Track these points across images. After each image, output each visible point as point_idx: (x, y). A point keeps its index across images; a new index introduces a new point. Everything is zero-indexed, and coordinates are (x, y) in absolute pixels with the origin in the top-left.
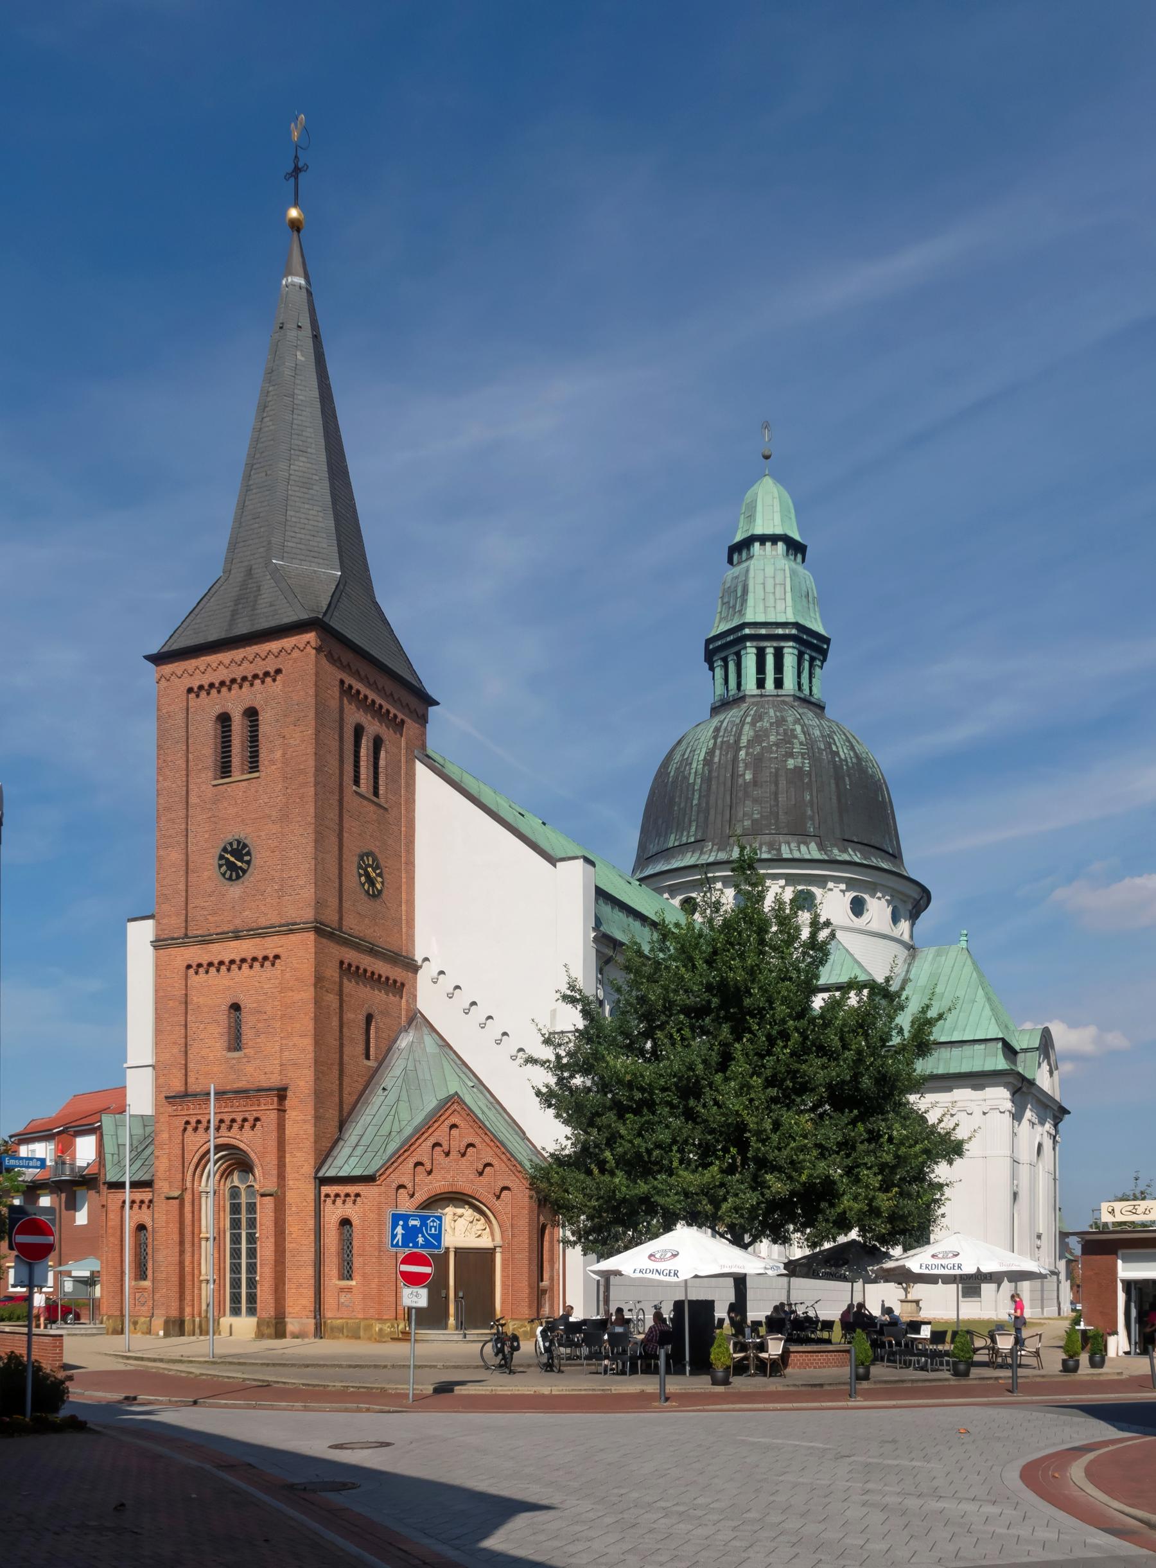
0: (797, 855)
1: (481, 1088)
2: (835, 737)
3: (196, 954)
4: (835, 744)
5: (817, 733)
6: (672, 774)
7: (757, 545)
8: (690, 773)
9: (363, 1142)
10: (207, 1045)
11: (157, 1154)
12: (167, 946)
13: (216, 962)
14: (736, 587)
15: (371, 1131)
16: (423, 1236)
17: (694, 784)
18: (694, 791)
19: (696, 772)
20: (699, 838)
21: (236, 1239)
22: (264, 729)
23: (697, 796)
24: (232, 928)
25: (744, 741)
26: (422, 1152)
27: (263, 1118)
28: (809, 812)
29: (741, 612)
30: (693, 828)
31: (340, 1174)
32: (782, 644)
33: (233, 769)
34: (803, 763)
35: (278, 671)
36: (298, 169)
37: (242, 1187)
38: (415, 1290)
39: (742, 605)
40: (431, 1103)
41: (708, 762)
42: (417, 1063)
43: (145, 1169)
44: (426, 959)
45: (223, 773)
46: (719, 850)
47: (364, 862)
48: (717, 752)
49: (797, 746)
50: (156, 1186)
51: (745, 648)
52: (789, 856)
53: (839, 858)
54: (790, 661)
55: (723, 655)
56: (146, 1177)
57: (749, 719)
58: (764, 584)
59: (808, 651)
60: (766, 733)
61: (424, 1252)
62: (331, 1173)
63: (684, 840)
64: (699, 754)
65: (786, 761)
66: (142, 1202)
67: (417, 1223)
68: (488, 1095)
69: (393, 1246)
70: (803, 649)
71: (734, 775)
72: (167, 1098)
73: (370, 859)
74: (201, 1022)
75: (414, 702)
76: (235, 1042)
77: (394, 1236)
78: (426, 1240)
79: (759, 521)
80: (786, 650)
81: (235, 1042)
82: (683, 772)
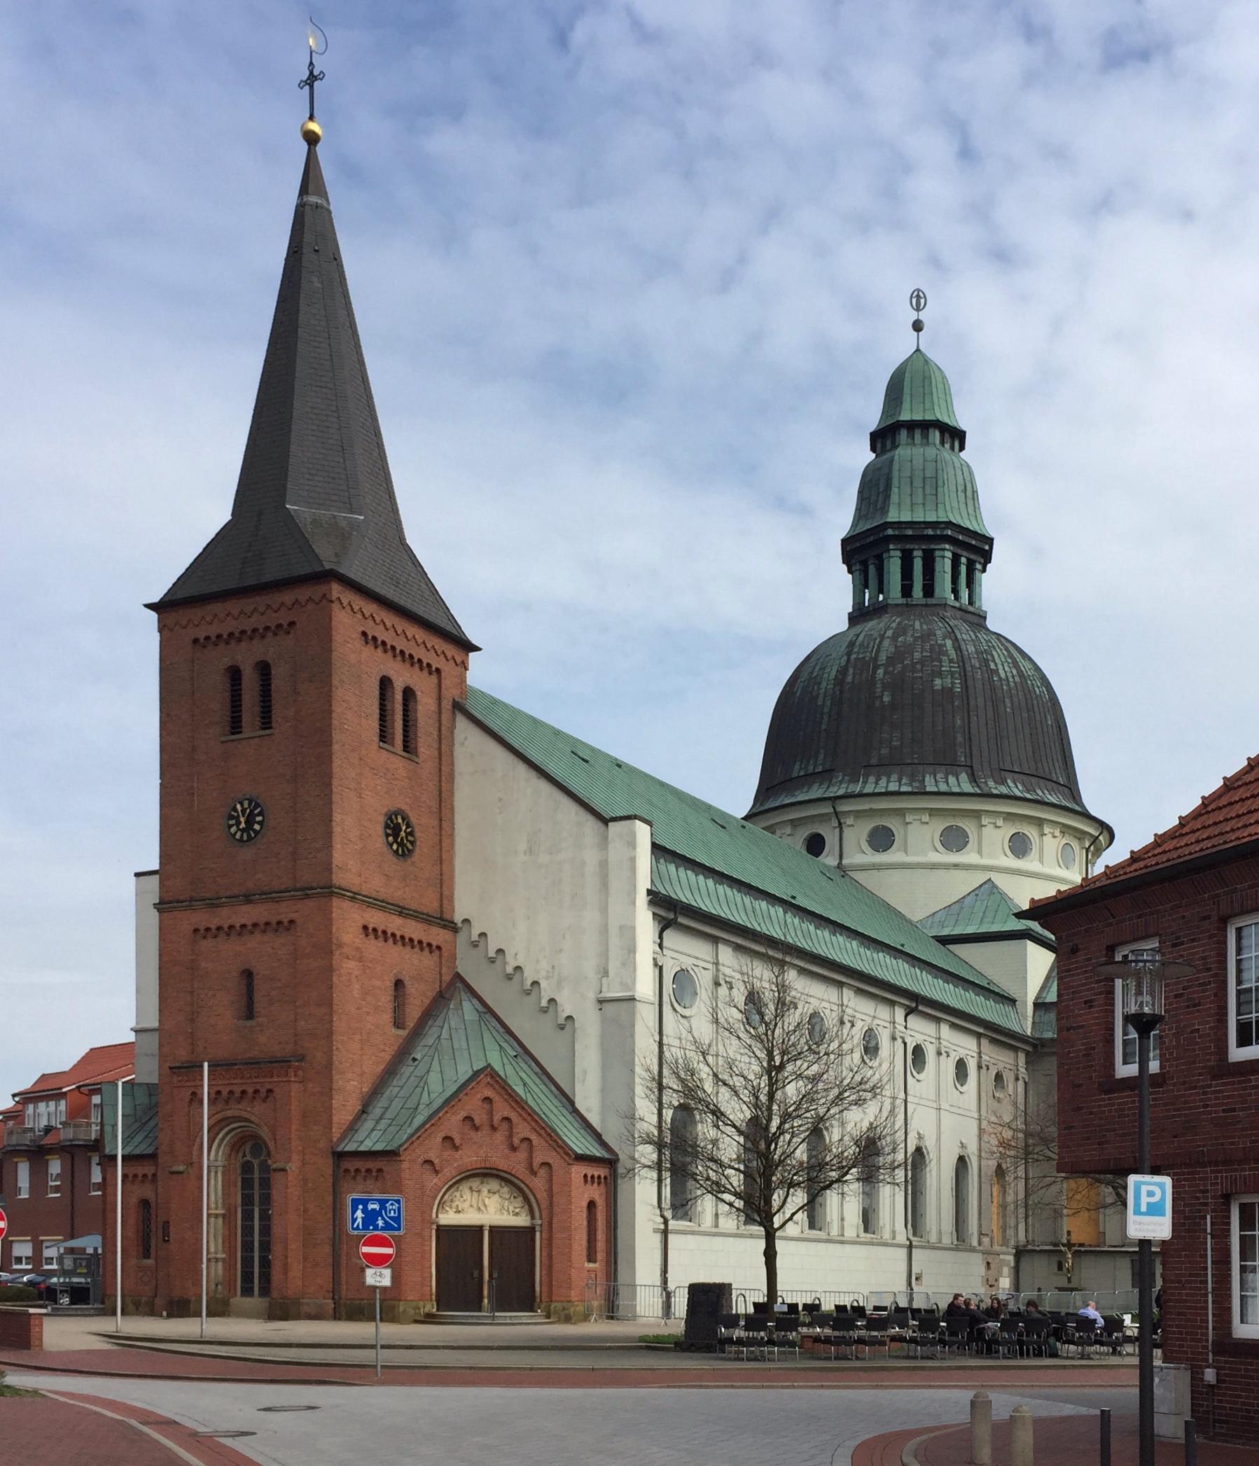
1: (527, 1058)
2: (994, 653)
3: (201, 918)
4: (994, 661)
5: (971, 649)
7: (904, 434)
10: (216, 1013)
11: (160, 1126)
12: (170, 910)
13: (226, 926)
14: (879, 480)
15: (397, 1104)
16: (383, 1219)
18: (822, 714)
20: (827, 767)
21: (247, 1216)
22: (275, 684)
27: (277, 1090)
29: (884, 510)
30: (821, 756)
31: (362, 1148)
32: (933, 546)
33: (244, 725)
34: (953, 683)
35: (292, 624)
36: (314, 76)
38: (379, 1270)
40: (464, 1072)
43: (149, 1141)
45: (233, 728)
46: (850, 781)
47: (392, 822)
48: (851, 671)
50: (160, 1160)
53: (995, 792)
56: (150, 1151)
57: (889, 633)
58: (911, 477)
59: (965, 553)
60: (910, 649)
61: (386, 1234)
62: (351, 1147)
64: (829, 673)
65: (932, 681)
67: (376, 1207)
68: (533, 1064)
69: (353, 1229)
70: (959, 551)
72: (171, 1068)
73: (399, 817)
75: (451, 650)
77: (354, 1220)
78: (386, 1222)
80: (916, 553)
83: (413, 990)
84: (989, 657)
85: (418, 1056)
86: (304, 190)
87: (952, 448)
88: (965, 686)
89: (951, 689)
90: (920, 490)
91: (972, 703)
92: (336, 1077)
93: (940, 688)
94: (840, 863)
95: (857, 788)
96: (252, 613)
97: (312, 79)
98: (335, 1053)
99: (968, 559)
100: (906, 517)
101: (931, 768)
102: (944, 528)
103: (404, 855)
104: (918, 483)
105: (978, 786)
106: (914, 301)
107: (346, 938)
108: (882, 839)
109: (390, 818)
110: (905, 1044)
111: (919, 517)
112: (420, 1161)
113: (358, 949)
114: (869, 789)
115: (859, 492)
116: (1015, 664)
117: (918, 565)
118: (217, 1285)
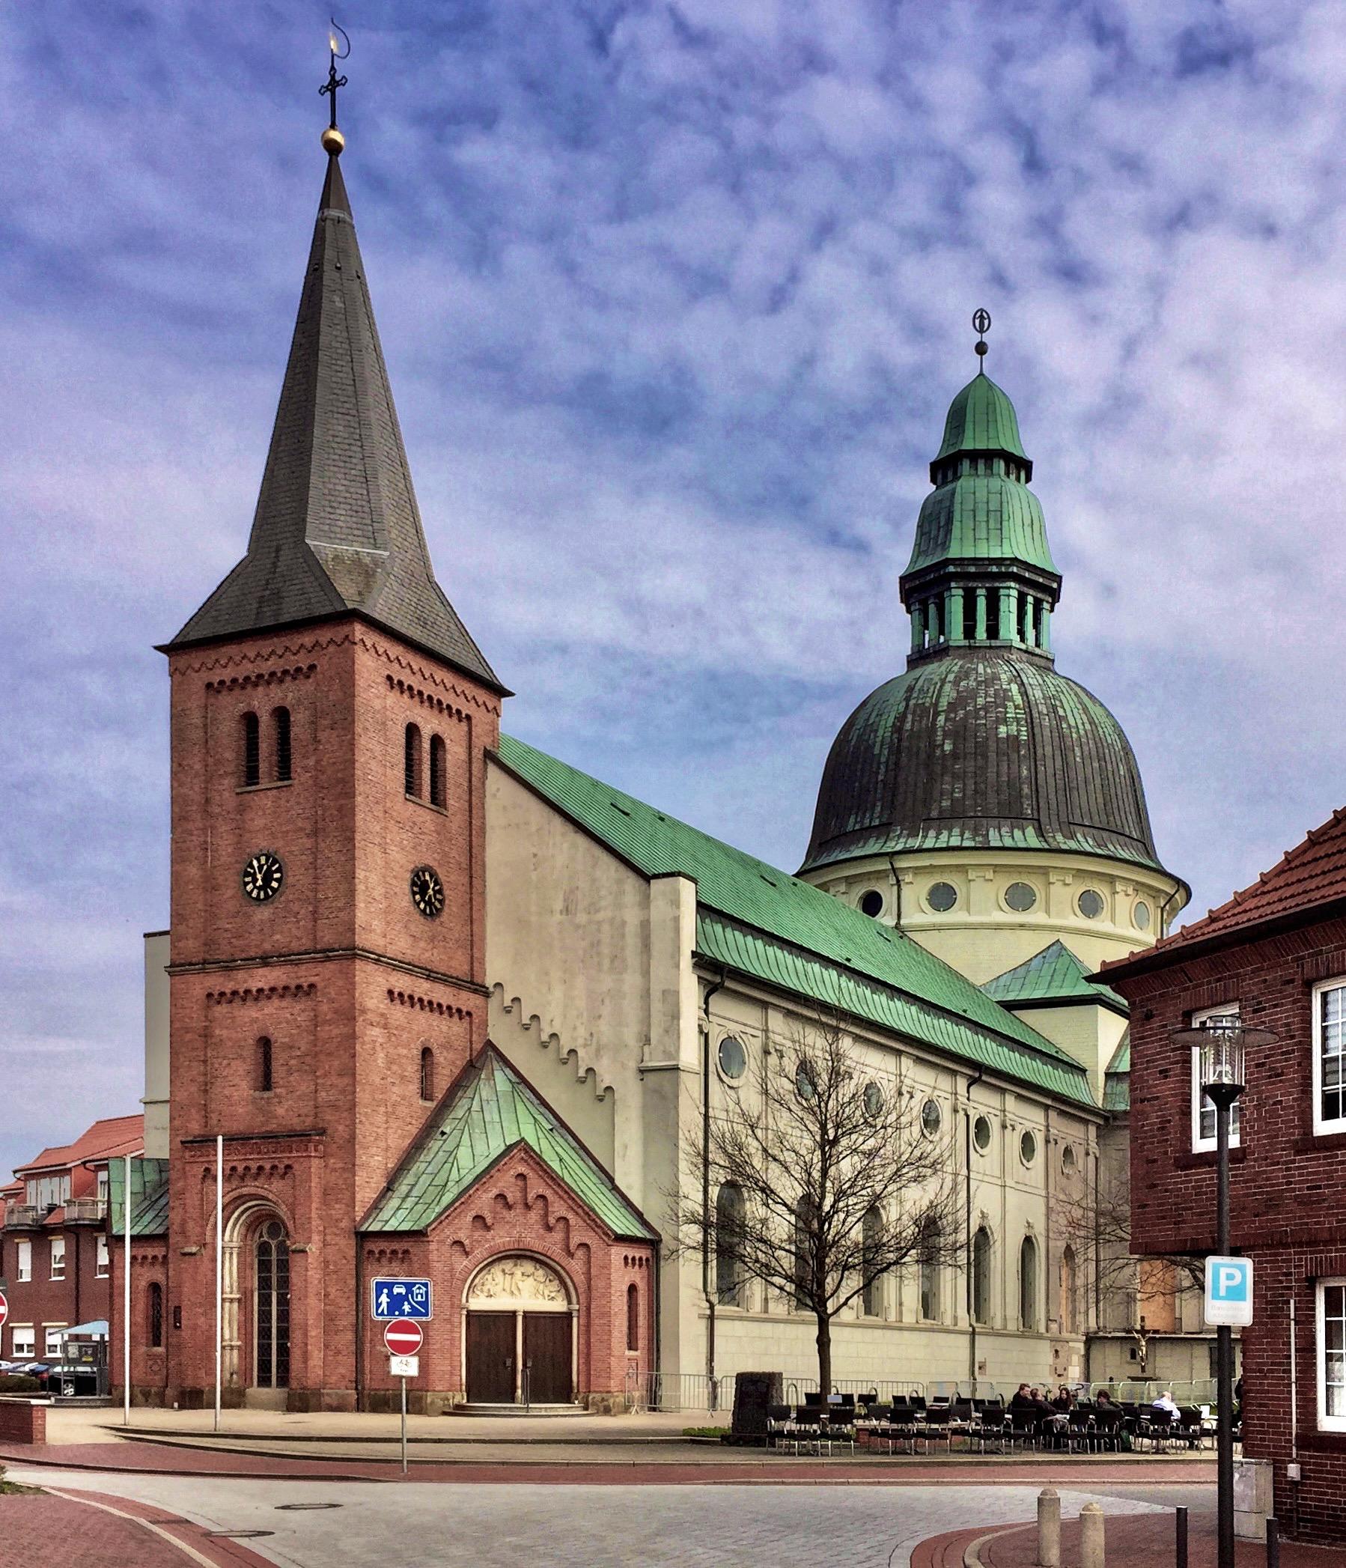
0: (1008, 842)
3: (217, 982)
4: (1063, 707)
5: (1038, 694)
6: (853, 743)
7: (966, 464)
8: (875, 743)
9: (415, 1193)
11: (171, 1204)
12: (182, 973)
15: (424, 1180)
16: (410, 1303)
17: (880, 754)
18: (879, 763)
19: (882, 742)
20: (884, 820)
21: (265, 1301)
23: (883, 768)
24: (260, 953)
25: (944, 704)
26: (484, 1201)
27: (296, 1166)
28: (1026, 790)
29: (945, 546)
31: (386, 1228)
32: (997, 584)
34: (1019, 731)
35: (312, 667)
37: (273, 1243)
39: (946, 536)
41: (898, 728)
42: (484, 1104)
44: (498, 985)
46: (909, 836)
47: (419, 878)
48: (910, 717)
49: (1011, 710)
51: (950, 589)
52: (1000, 844)
53: (1064, 847)
54: (1009, 606)
55: (923, 596)
57: (951, 677)
58: (974, 511)
59: (1031, 592)
60: (973, 694)
61: (413, 1320)
62: (375, 1227)
63: (867, 822)
64: (886, 720)
65: (997, 728)
66: (155, 1257)
67: (403, 1291)
69: (378, 1314)
70: (1026, 590)
71: (932, 746)
72: (182, 1142)
73: (427, 874)
74: (224, 1058)
76: (266, 1082)
77: (378, 1305)
79: (969, 432)
80: (979, 592)
81: (266, 1082)
82: (867, 741)
83: (442, 1059)
84: (1058, 703)
85: (447, 1130)
86: (325, 203)
87: (1018, 479)
88: (1032, 734)
89: (1017, 737)
90: (984, 525)
91: (1040, 751)
92: (359, 1152)
93: (1005, 735)
94: (898, 923)
95: (915, 843)
96: (269, 656)
97: (333, 85)
98: (358, 1126)
99: (1035, 598)
100: (969, 553)
101: (996, 822)
102: (1010, 565)
103: (431, 914)
104: (981, 517)
105: (1046, 841)
106: (977, 322)
107: (370, 1004)
108: (942, 898)
109: (417, 875)
110: (968, 1116)
111: (983, 552)
112: (449, 1241)
113: (382, 1015)
114: (929, 843)
115: (918, 526)
116: (1086, 710)
117: (982, 605)
118: (232, 1374)
